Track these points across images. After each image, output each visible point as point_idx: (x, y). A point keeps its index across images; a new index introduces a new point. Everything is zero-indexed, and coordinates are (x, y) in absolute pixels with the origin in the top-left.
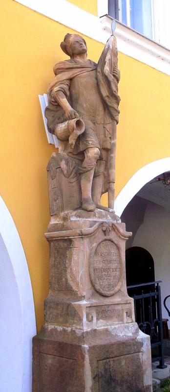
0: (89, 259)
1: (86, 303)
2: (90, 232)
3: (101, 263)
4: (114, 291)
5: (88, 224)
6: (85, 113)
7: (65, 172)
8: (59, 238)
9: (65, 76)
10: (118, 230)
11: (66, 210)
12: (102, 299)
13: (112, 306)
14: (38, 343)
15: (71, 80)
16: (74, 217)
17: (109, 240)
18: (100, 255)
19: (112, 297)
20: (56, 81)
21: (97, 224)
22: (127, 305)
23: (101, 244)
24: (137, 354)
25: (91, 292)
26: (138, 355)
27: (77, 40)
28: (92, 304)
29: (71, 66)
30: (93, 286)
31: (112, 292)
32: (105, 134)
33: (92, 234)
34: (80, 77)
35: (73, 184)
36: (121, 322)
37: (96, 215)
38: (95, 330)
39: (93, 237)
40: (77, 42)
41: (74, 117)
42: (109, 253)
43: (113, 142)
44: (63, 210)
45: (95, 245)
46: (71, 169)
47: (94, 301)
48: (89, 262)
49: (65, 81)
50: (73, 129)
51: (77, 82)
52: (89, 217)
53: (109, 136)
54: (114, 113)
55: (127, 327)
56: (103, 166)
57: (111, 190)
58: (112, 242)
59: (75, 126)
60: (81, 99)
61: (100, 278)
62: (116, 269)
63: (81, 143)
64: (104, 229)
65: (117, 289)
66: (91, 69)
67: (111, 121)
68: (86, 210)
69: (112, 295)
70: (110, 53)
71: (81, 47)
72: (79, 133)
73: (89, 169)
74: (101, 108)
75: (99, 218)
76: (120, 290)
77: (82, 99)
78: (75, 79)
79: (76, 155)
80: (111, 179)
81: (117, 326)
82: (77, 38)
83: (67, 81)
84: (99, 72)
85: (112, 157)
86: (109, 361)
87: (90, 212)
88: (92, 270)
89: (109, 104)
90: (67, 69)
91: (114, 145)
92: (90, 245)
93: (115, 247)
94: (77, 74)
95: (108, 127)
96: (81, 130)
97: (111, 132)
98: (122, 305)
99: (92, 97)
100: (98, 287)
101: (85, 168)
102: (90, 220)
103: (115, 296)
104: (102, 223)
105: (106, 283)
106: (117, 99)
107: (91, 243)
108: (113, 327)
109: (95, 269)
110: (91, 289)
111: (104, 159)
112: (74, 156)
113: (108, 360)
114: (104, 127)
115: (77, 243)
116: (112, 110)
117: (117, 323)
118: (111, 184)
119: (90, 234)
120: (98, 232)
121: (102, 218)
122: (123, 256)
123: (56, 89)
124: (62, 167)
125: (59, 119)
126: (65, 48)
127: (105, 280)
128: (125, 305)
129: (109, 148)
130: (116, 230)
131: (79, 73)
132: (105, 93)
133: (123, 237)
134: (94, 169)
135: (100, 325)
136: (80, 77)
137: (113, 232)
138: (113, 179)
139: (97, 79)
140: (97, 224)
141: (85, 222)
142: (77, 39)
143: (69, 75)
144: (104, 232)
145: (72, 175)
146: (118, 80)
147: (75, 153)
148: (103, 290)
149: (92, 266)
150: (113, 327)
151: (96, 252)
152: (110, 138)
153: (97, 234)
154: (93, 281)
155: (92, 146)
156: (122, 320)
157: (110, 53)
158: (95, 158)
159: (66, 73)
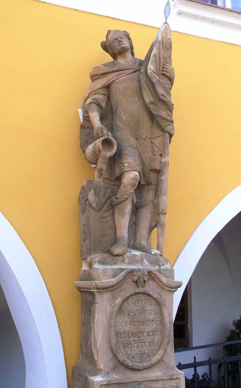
0: (109, 321)
1: (102, 379)
2: (110, 284)
3: (129, 325)
4: (150, 362)
5: (110, 273)
6: (125, 127)
7: (94, 205)
8: (84, 290)
10: (159, 279)
11: (94, 253)
15: (108, 87)
16: (97, 263)
17: (144, 293)
18: (127, 314)
19: (148, 371)
20: (89, 92)
21: (123, 273)
22: (174, 381)
23: (130, 299)
25: (111, 364)
27: (116, 37)
28: (110, 381)
29: (106, 71)
30: (115, 356)
31: (146, 364)
32: (153, 151)
33: (115, 287)
34: (118, 83)
35: (107, 219)
37: (126, 261)
39: (119, 289)
40: (117, 39)
41: (100, 135)
42: (142, 311)
43: (163, 160)
44: (90, 254)
45: (119, 301)
46: (103, 200)
47: (115, 377)
48: (109, 324)
49: (100, 90)
50: (100, 152)
51: (114, 87)
52: (115, 264)
53: (160, 153)
54: (163, 124)
56: (152, 192)
57: (121, 238)
58: (149, 295)
59: (101, 147)
60: (120, 109)
61: (126, 345)
62: (154, 332)
63: (116, 166)
64: (135, 278)
65: (155, 359)
66: (132, 71)
67: (161, 133)
68: (112, 254)
69: (148, 368)
70: (164, 46)
71: (120, 45)
72: (110, 154)
73: (122, 200)
74: (146, 119)
75: (129, 263)
76: (160, 361)
77: (121, 110)
78: (112, 86)
79: (114, 181)
80: (161, 210)
82: (117, 34)
84: (142, 73)
85: (162, 180)
87: (118, 257)
88: (113, 335)
89: (155, 113)
90: (103, 74)
91: (166, 164)
92: (112, 302)
93: (154, 303)
94: (114, 79)
95: (157, 142)
96: (112, 151)
97: (162, 148)
98: (164, 382)
99: (132, 106)
100: (121, 357)
101: (118, 198)
102: (115, 267)
103: (152, 369)
104: (132, 272)
105: (135, 351)
106: (169, 107)
107: (114, 298)
109: (118, 334)
110: (112, 360)
111: (153, 184)
112: (112, 183)
114: (152, 143)
115: (98, 297)
116: (159, 120)
118: (160, 215)
119: (113, 286)
120: (126, 283)
121: (133, 264)
123: (89, 101)
124: (89, 199)
125: (92, 138)
126: (105, 47)
128: (169, 381)
129: (158, 169)
131: (116, 78)
132: (148, 98)
133: (167, 288)
134: (130, 198)
136: (118, 83)
137: (151, 282)
138: (163, 210)
139: (139, 81)
140: (123, 273)
141: (104, 271)
142: (116, 36)
143: (104, 82)
144: (136, 282)
145: (105, 208)
146: (171, 80)
147: (113, 179)
148: (132, 361)
149: (113, 329)
151: (120, 310)
152: (161, 155)
153: (124, 286)
154: (114, 350)
155: (128, 169)
157: (164, 46)
158: (133, 185)
159: (100, 80)
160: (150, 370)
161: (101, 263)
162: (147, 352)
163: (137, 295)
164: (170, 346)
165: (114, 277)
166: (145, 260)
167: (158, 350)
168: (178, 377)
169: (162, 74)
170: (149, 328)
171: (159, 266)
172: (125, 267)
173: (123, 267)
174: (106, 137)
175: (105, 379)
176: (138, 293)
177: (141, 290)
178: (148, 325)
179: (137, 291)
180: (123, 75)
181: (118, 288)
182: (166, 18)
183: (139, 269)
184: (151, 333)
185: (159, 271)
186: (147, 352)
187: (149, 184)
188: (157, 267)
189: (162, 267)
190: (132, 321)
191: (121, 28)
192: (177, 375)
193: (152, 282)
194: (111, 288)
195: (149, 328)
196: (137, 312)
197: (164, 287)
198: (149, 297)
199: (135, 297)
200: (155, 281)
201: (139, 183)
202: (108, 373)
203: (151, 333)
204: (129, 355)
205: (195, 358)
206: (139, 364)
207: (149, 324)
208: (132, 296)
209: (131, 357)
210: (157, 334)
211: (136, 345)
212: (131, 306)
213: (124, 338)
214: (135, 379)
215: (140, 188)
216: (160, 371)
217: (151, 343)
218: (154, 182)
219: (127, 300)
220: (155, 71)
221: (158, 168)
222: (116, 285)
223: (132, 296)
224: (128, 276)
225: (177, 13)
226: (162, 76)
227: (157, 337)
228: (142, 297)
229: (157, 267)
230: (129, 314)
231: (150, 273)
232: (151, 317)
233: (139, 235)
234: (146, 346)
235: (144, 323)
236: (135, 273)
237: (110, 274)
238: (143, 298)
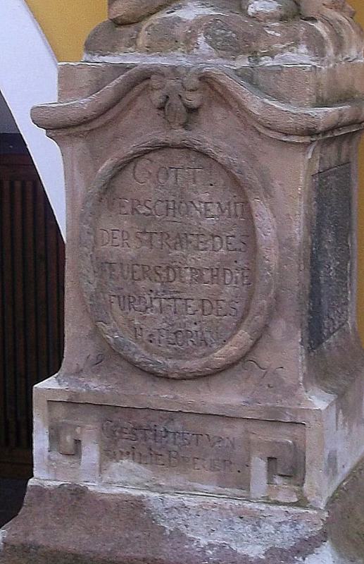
3: (134, 243)
4: (204, 360)
12: (138, 382)
13: (188, 419)
17: (185, 147)
18: (128, 209)
19: (201, 385)
22: (284, 429)
23: (143, 163)
28: (77, 395)
31: (193, 364)
36: (237, 492)
37: (140, 42)
38: (78, 493)
39: (110, 133)
45: (106, 165)
55: (256, 520)
58: (204, 154)
62: (218, 273)
65: (220, 355)
75: (149, 49)
81: (191, 502)
98: (251, 426)
103: (214, 381)
104: (145, 76)
107: (96, 158)
108: (172, 499)
117: (211, 488)
119: (85, 121)
120: (132, 113)
122: (356, 247)
127: (150, 314)
130: (233, 104)
135: (121, 480)
137: (219, 113)
148: (147, 348)
150: (172, 499)
156: (243, 483)
162: (194, 328)
163: (165, 151)
164: (282, 324)
165: (321, 103)
166: (201, 39)
167: (238, 327)
168: (299, 420)
170: (200, 258)
171: (254, 55)
175: (64, 387)
176: (164, 147)
177: (178, 135)
178: (197, 248)
179: (162, 139)
181: (106, 124)
183: (174, 68)
184: (207, 275)
185: (248, 77)
186: (194, 328)
188: (243, 62)
189: (267, 62)
190: (144, 232)
192: (296, 412)
193: (222, 110)
194: (83, 128)
195: (200, 258)
196: (161, 206)
197: (262, 131)
198: (203, 161)
199: (157, 157)
200: (231, 108)
202: (79, 372)
203: (207, 275)
204: (139, 332)
206: (170, 363)
207: (201, 246)
208: (147, 152)
209: (145, 337)
210: (228, 277)
212: (141, 183)
213: (121, 279)
214: (154, 404)
216: (241, 393)
219: (132, 165)
223: (147, 152)
224: (136, 90)
227: (228, 289)
229: (243, 62)
230: (134, 210)
231: (206, 80)
232: (208, 224)
235: (181, 239)
236: (154, 82)
238: (184, 162)
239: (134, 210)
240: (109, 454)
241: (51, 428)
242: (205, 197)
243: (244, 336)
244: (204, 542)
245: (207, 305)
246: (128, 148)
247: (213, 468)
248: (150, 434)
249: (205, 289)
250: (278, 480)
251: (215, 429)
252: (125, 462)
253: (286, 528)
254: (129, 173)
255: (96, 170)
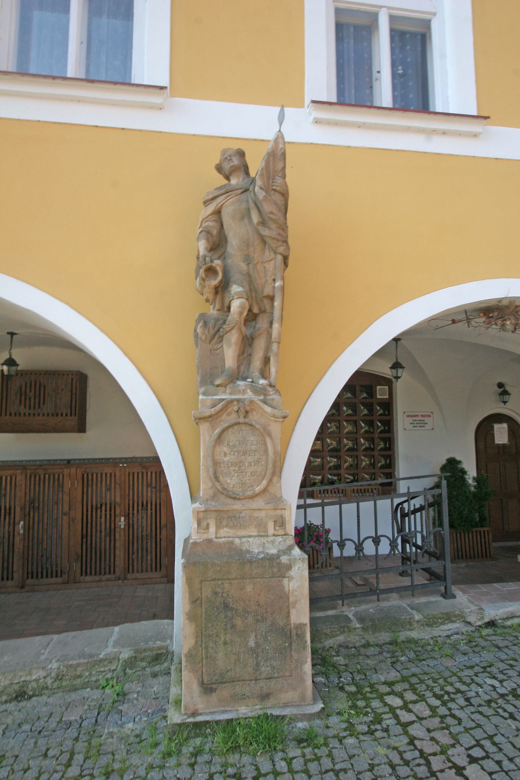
5: (209, 403)
9: (212, 208)
14: (173, 619)
17: (246, 424)
18: (226, 444)
21: (224, 402)
23: (231, 429)
24: (280, 579)
26: (282, 581)
46: (212, 332)
49: (210, 217)
53: (272, 278)
58: (251, 425)
65: (258, 489)
66: (241, 191)
75: (231, 394)
83: (214, 216)
86: (223, 584)
93: (244, 425)
94: (222, 203)
107: (213, 428)
111: (268, 311)
113: (220, 582)
131: (224, 201)
160: (253, 500)
161: (204, 394)
166: (249, 391)
167: (263, 480)
169: (273, 189)
172: (226, 397)
173: (223, 397)
174: (209, 265)
177: (241, 420)
178: (250, 455)
180: (231, 196)
182: (281, 124)
184: (253, 464)
187: (263, 311)
191: (235, 146)
196: (237, 443)
201: (250, 310)
203: (253, 464)
205: (408, 489)
211: (236, 474)
212: (232, 437)
215: (251, 317)
217: (253, 474)
218: (268, 309)
220: (263, 187)
221: (271, 294)
222: (214, 415)
225: (313, 122)
226: (273, 192)
228: (244, 427)
229: (262, 397)
230: (228, 444)
232: (253, 447)
233: (252, 366)
234: (247, 476)
235: (244, 453)
237: (209, 404)
239: (228, 444)
240: (218, 527)
241: (198, 521)
242: (252, 439)
243: (265, 482)
244: (256, 551)
245: (253, 473)
246: (225, 425)
247: (255, 527)
248: (233, 519)
249: (252, 469)
250: (277, 528)
251: (256, 514)
252: (225, 529)
253: (282, 543)
254: (226, 433)
255: (213, 432)
